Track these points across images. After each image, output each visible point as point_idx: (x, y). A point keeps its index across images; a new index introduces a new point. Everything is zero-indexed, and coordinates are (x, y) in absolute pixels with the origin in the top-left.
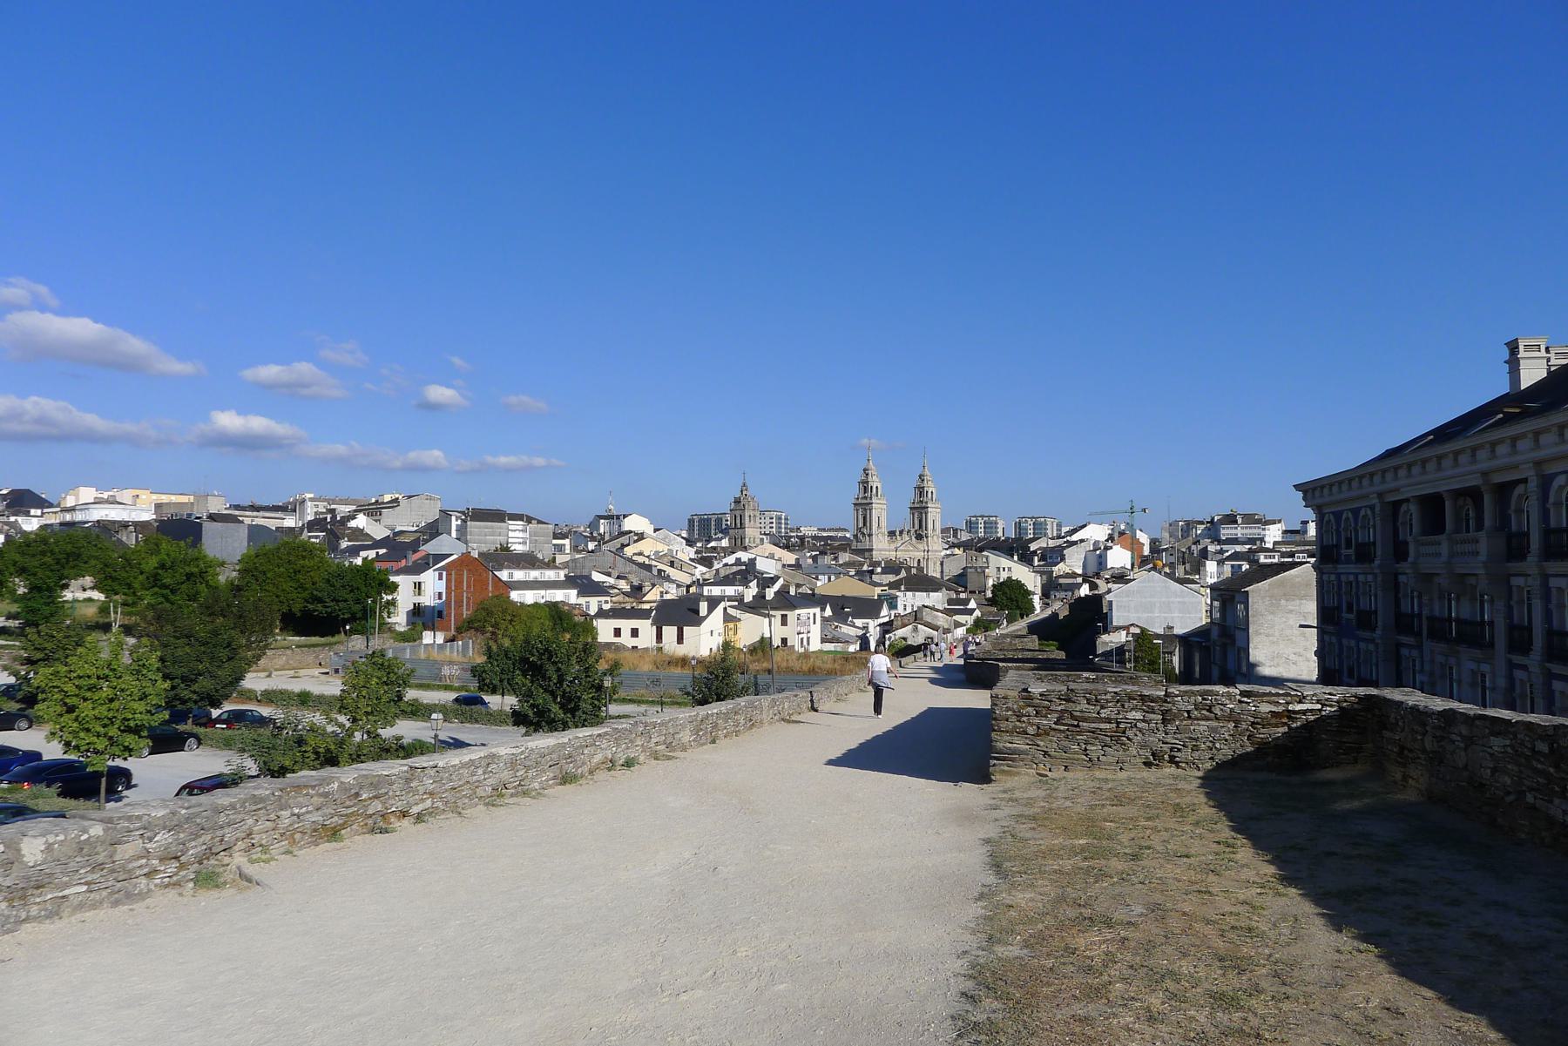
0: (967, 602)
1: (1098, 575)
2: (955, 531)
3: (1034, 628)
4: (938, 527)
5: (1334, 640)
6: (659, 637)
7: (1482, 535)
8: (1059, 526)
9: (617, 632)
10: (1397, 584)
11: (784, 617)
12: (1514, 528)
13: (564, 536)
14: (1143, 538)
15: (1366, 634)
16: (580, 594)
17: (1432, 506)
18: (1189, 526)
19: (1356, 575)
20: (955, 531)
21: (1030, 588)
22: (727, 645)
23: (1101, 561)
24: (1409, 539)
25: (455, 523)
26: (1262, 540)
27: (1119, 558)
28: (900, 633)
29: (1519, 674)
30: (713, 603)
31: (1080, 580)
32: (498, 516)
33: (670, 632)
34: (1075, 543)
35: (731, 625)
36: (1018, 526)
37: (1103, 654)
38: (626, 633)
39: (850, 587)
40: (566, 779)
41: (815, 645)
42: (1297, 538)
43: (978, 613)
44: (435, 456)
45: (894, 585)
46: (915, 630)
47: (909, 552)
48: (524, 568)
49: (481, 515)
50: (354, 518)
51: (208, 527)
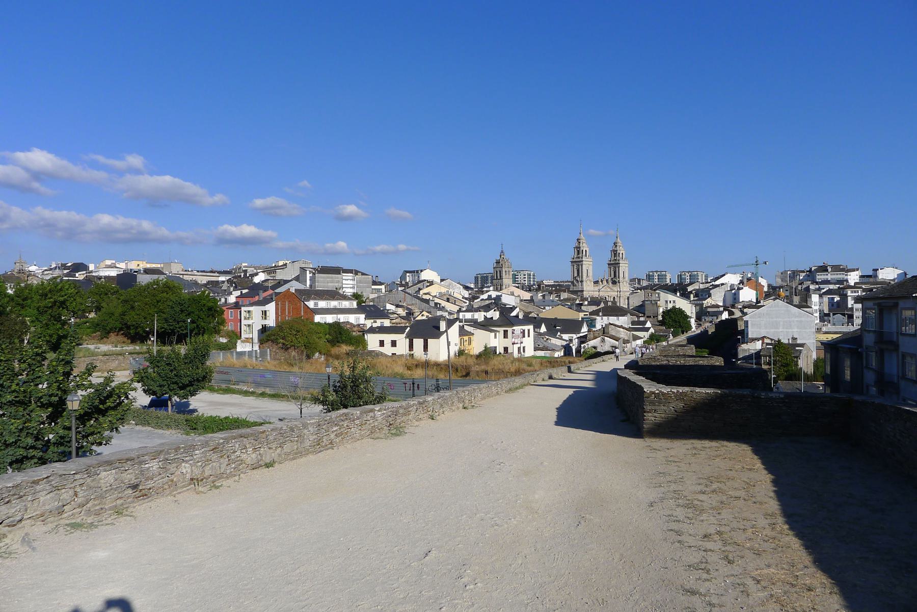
0: (644, 323)
1: (733, 306)
2: (639, 280)
3: (691, 340)
4: (627, 279)
6: (411, 347)
9: (382, 343)
11: (506, 332)
13: (381, 284)
14: (763, 282)
18: (795, 274)
20: (639, 280)
21: (689, 314)
22: (461, 353)
23: (736, 297)
25: (309, 275)
26: (847, 281)
27: (747, 295)
28: (592, 343)
30: (450, 323)
31: (721, 309)
32: (337, 271)
33: (418, 343)
34: (718, 286)
35: (466, 338)
37: (743, 358)
38: (388, 343)
39: (564, 313)
41: (530, 352)
42: (871, 280)
43: (652, 330)
44: (342, 245)
45: (596, 313)
46: (603, 341)
47: (607, 292)
48: (326, 299)
49: (325, 270)
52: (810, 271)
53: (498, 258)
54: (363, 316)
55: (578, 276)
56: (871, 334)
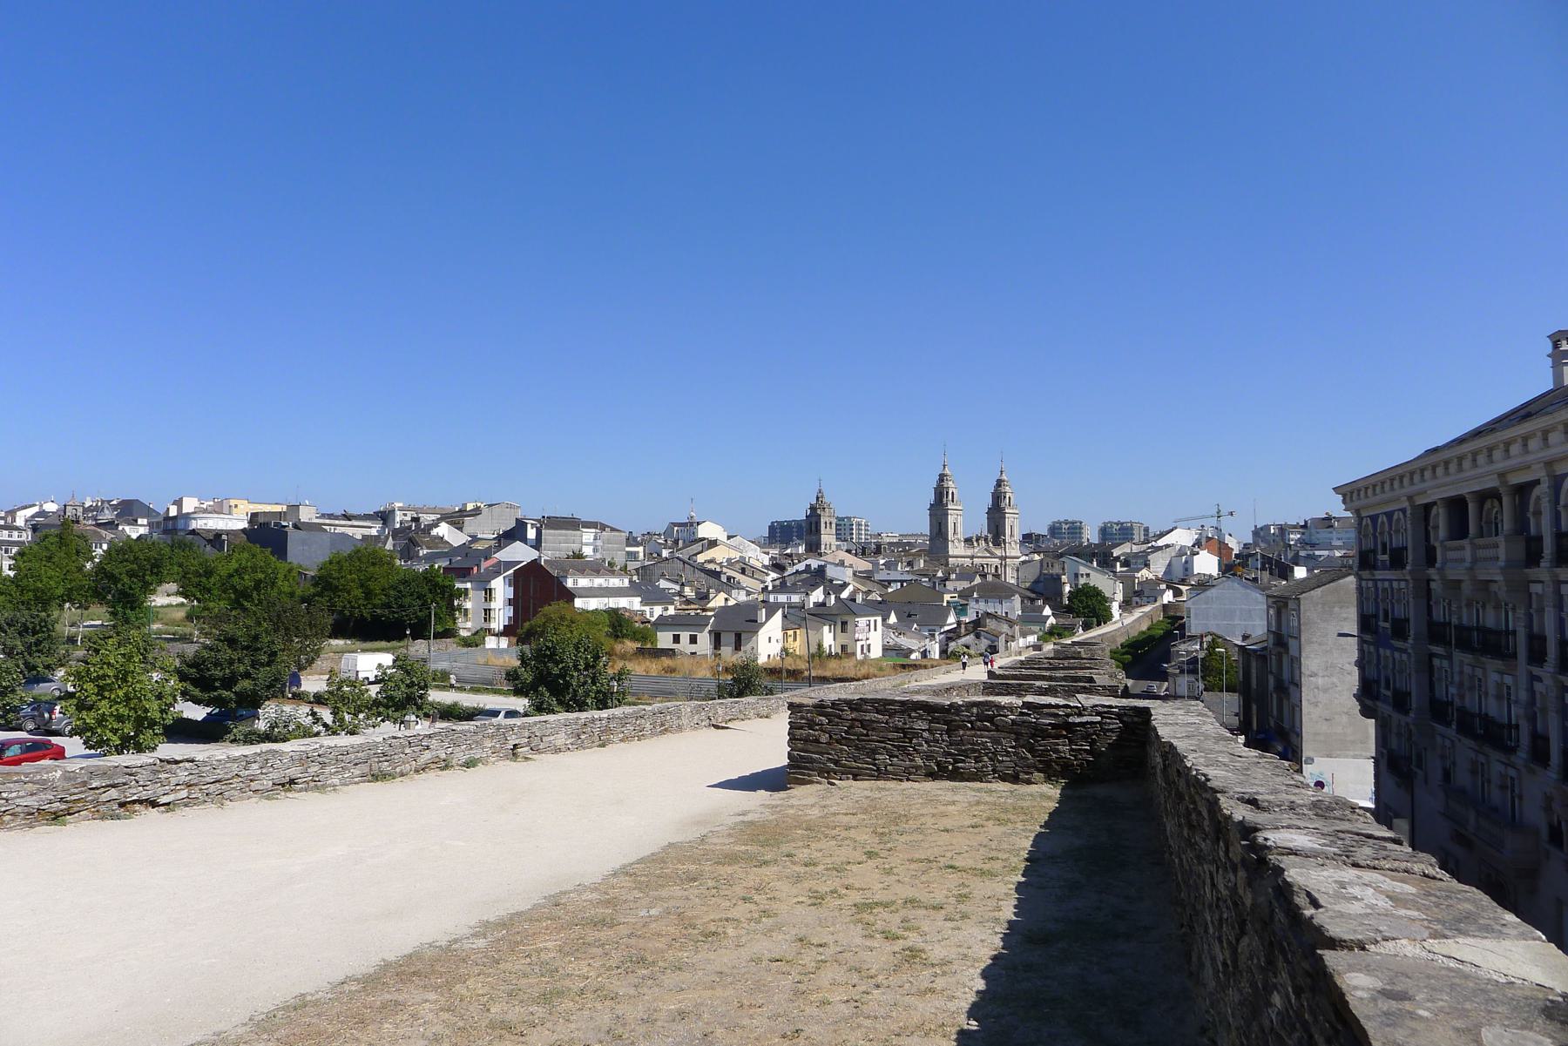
4: (1018, 537)
5: (1372, 649)
7: (1501, 540)
9: (676, 639)
10: (1429, 590)
12: (1533, 531)
13: (638, 545)
15: (1398, 644)
16: (643, 603)
17: (1457, 506)
19: (1390, 581)
24: (1437, 544)
29: (1538, 686)
31: (1163, 586)
32: (573, 524)
34: (1160, 548)
40: (377, 777)
50: (436, 526)
51: (293, 537)
52: (1305, 526)
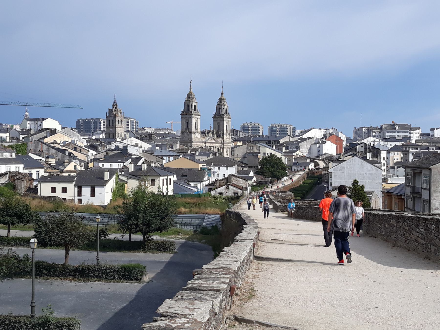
4: (229, 129)
6: (80, 194)
8: (294, 129)
9: (53, 190)
11: (398, 159)
14: (343, 137)
20: (236, 131)
34: (305, 140)
36: (271, 129)
39: (183, 163)
43: (255, 179)
46: (228, 188)
47: (212, 143)
52: (381, 128)
53: (111, 108)
54: (21, 166)
55: (187, 129)
56: (409, 188)
